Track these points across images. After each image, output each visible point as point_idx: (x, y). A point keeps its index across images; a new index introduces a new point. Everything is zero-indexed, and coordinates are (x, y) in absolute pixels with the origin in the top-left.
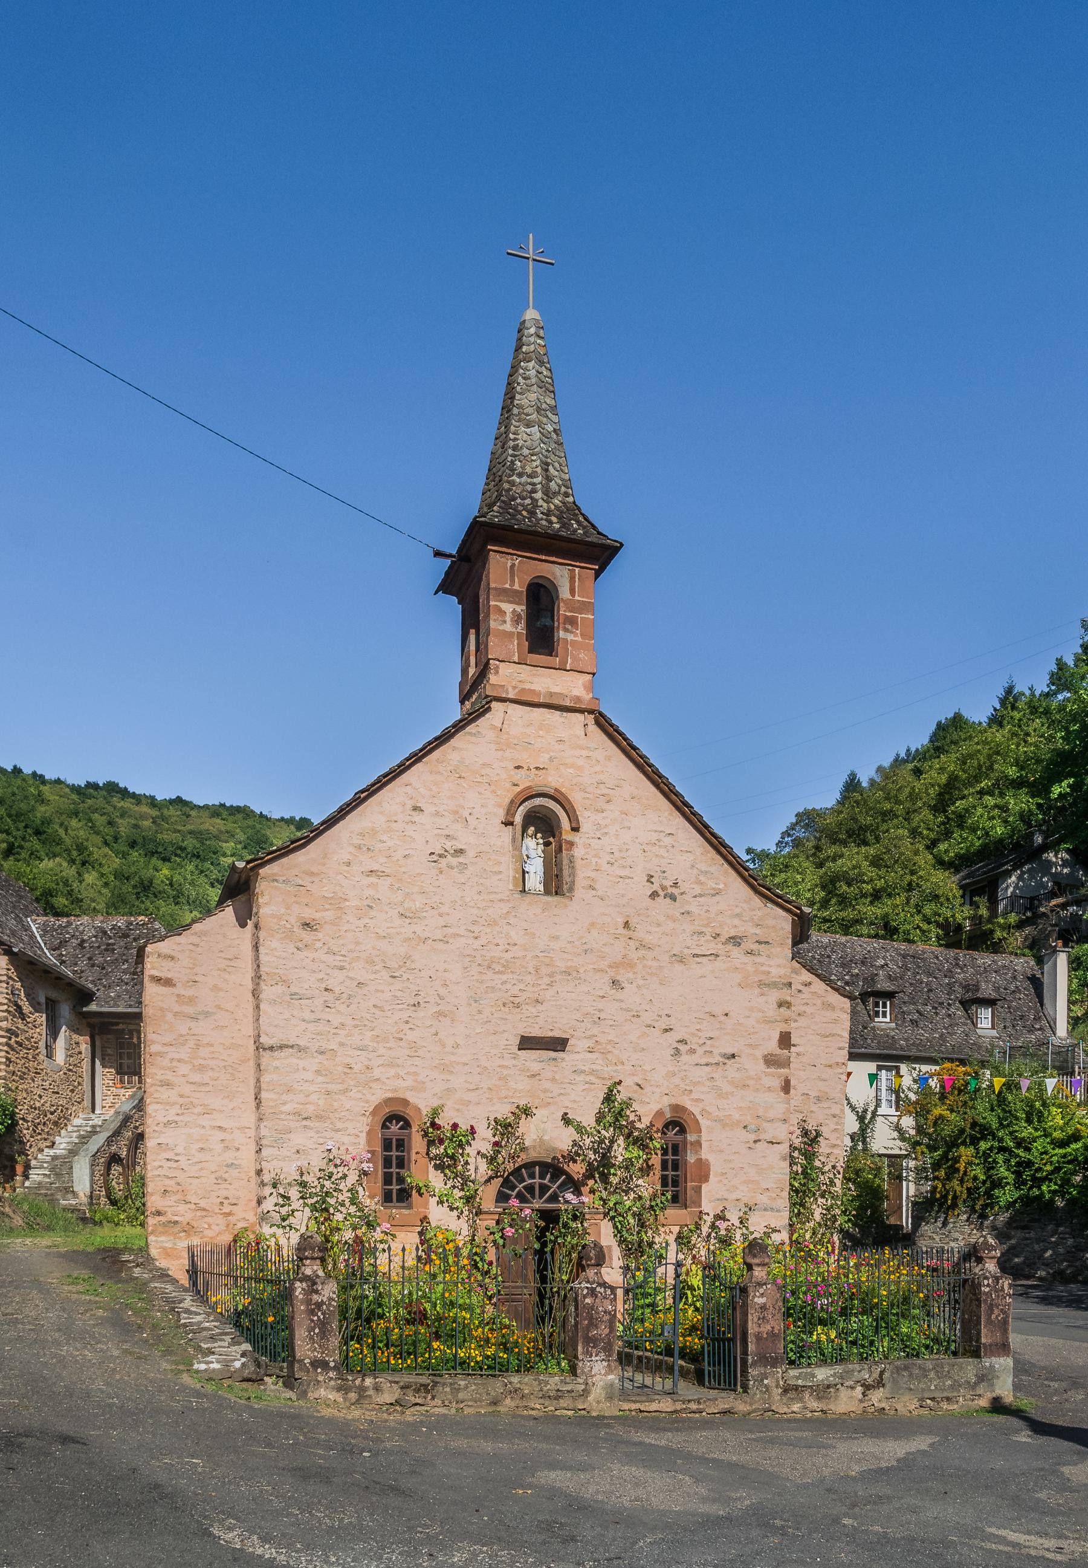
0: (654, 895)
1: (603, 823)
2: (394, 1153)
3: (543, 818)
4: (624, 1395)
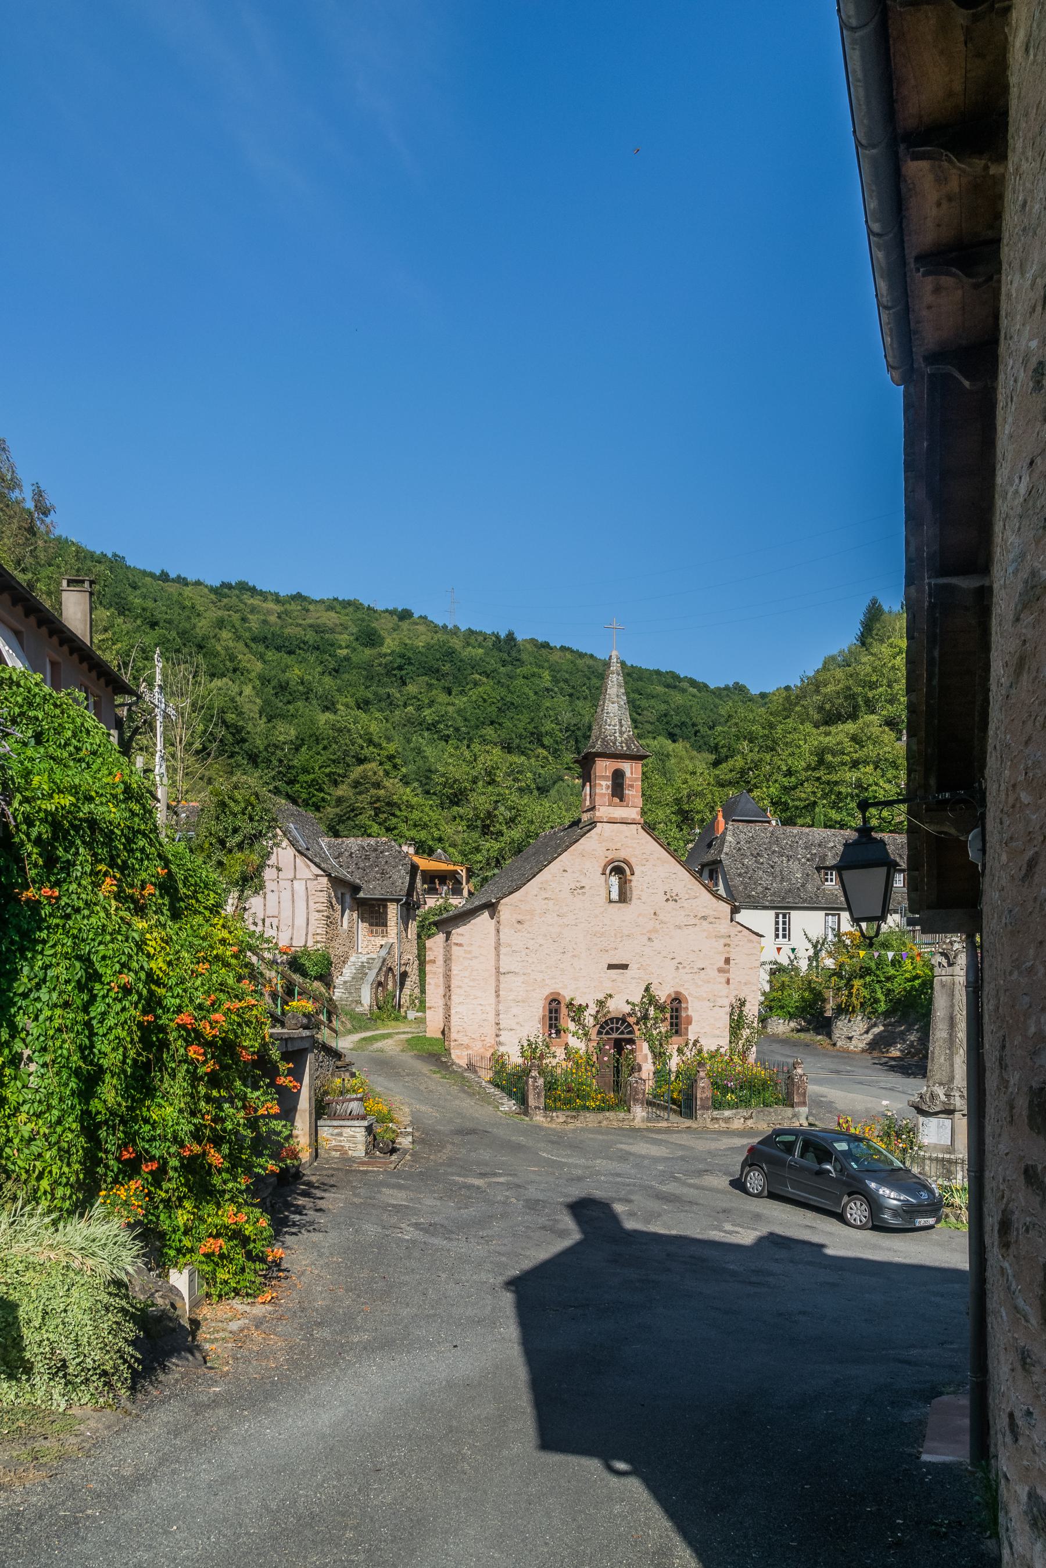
0: (667, 900)
3: (619, 870)
4: (648, 1120)
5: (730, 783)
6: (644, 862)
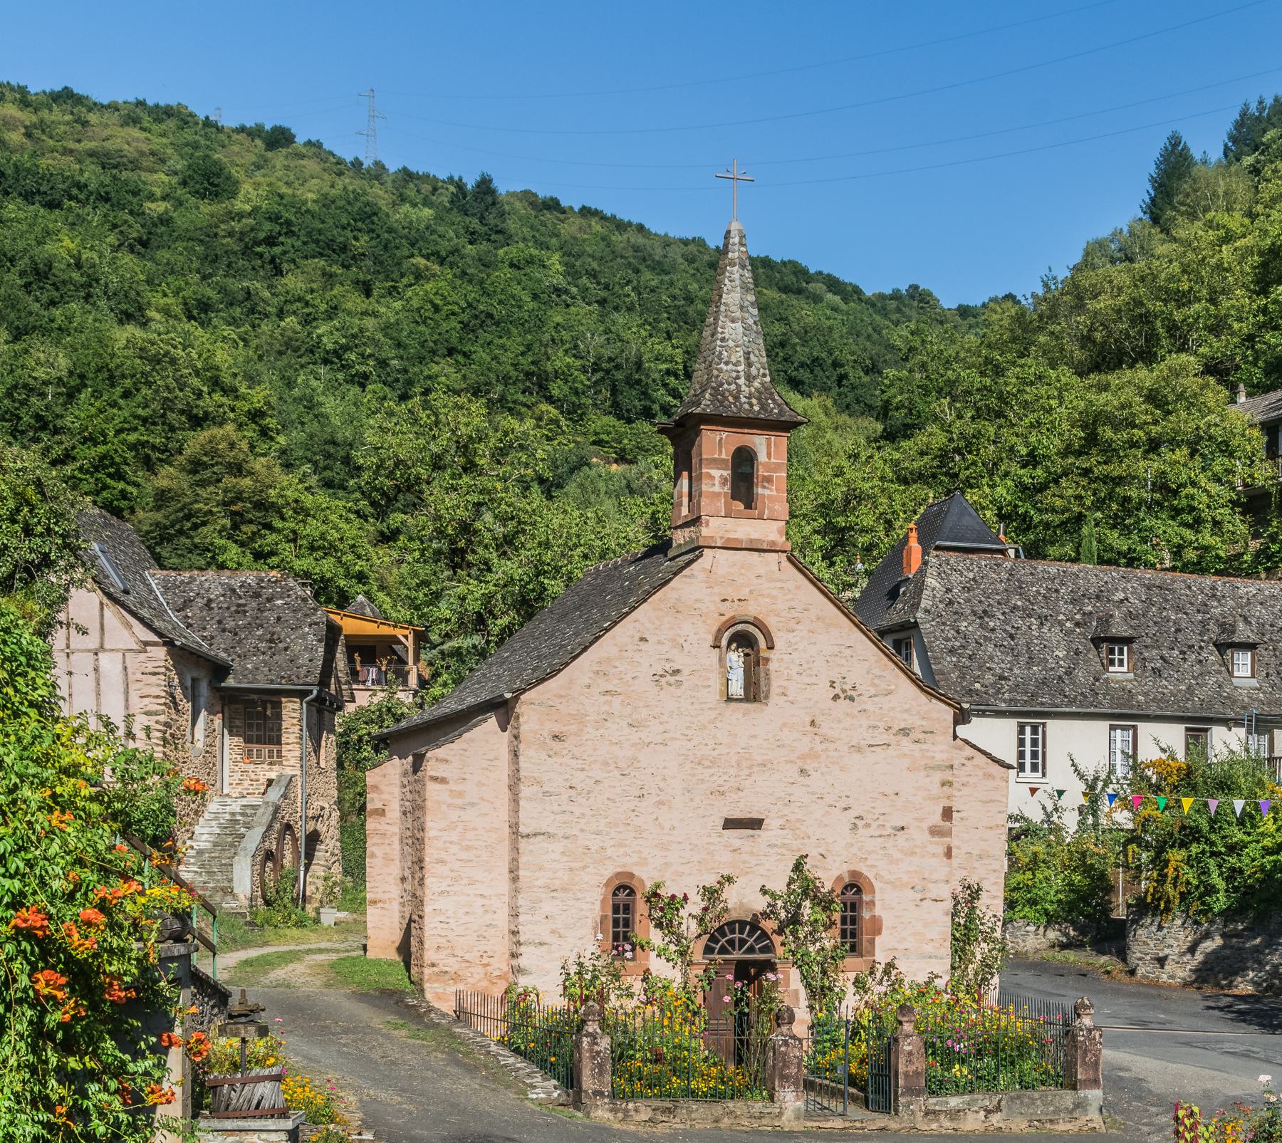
0: (836, 697)
1: (793, 641)
2: (621, 916)
3: (746, 639)
4: (808, 1115)
5: (921, 476)
6: (792, 624)
